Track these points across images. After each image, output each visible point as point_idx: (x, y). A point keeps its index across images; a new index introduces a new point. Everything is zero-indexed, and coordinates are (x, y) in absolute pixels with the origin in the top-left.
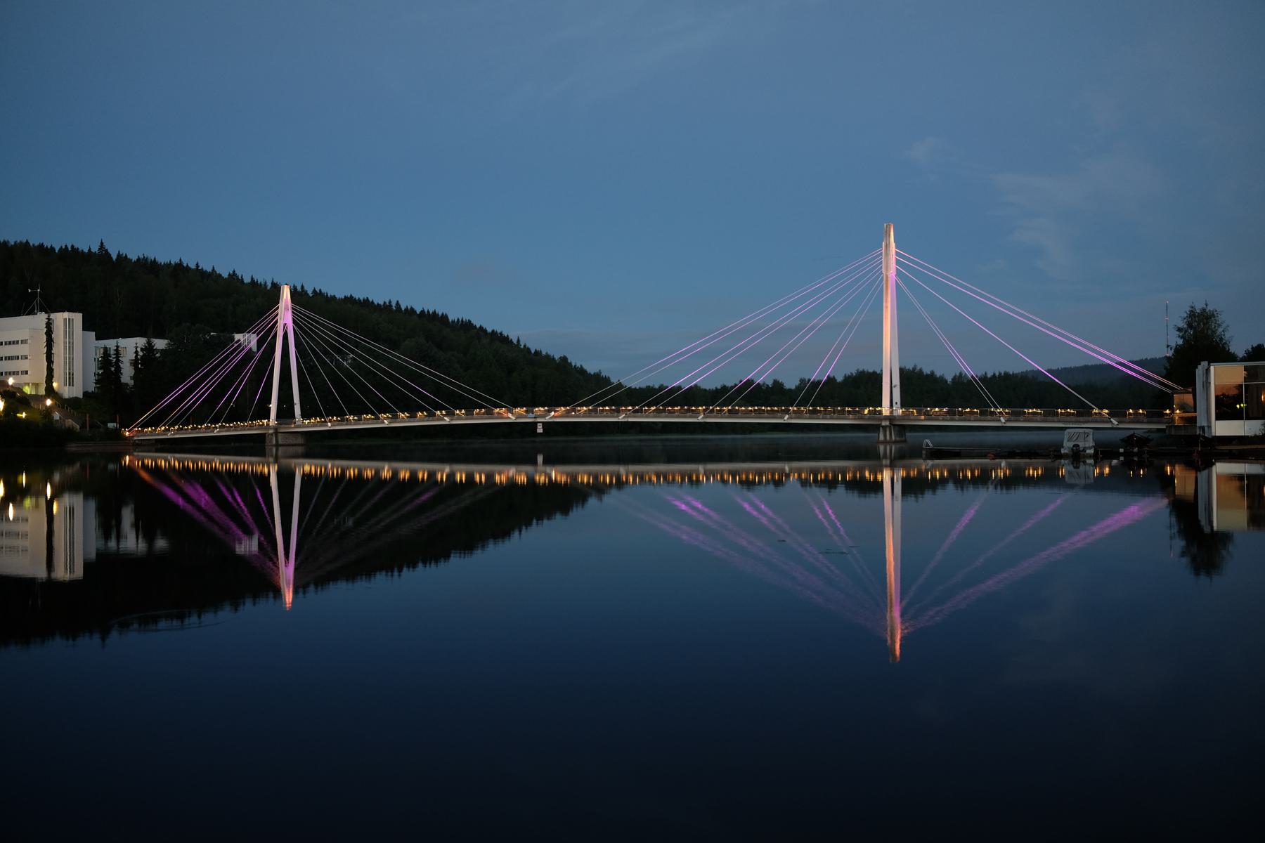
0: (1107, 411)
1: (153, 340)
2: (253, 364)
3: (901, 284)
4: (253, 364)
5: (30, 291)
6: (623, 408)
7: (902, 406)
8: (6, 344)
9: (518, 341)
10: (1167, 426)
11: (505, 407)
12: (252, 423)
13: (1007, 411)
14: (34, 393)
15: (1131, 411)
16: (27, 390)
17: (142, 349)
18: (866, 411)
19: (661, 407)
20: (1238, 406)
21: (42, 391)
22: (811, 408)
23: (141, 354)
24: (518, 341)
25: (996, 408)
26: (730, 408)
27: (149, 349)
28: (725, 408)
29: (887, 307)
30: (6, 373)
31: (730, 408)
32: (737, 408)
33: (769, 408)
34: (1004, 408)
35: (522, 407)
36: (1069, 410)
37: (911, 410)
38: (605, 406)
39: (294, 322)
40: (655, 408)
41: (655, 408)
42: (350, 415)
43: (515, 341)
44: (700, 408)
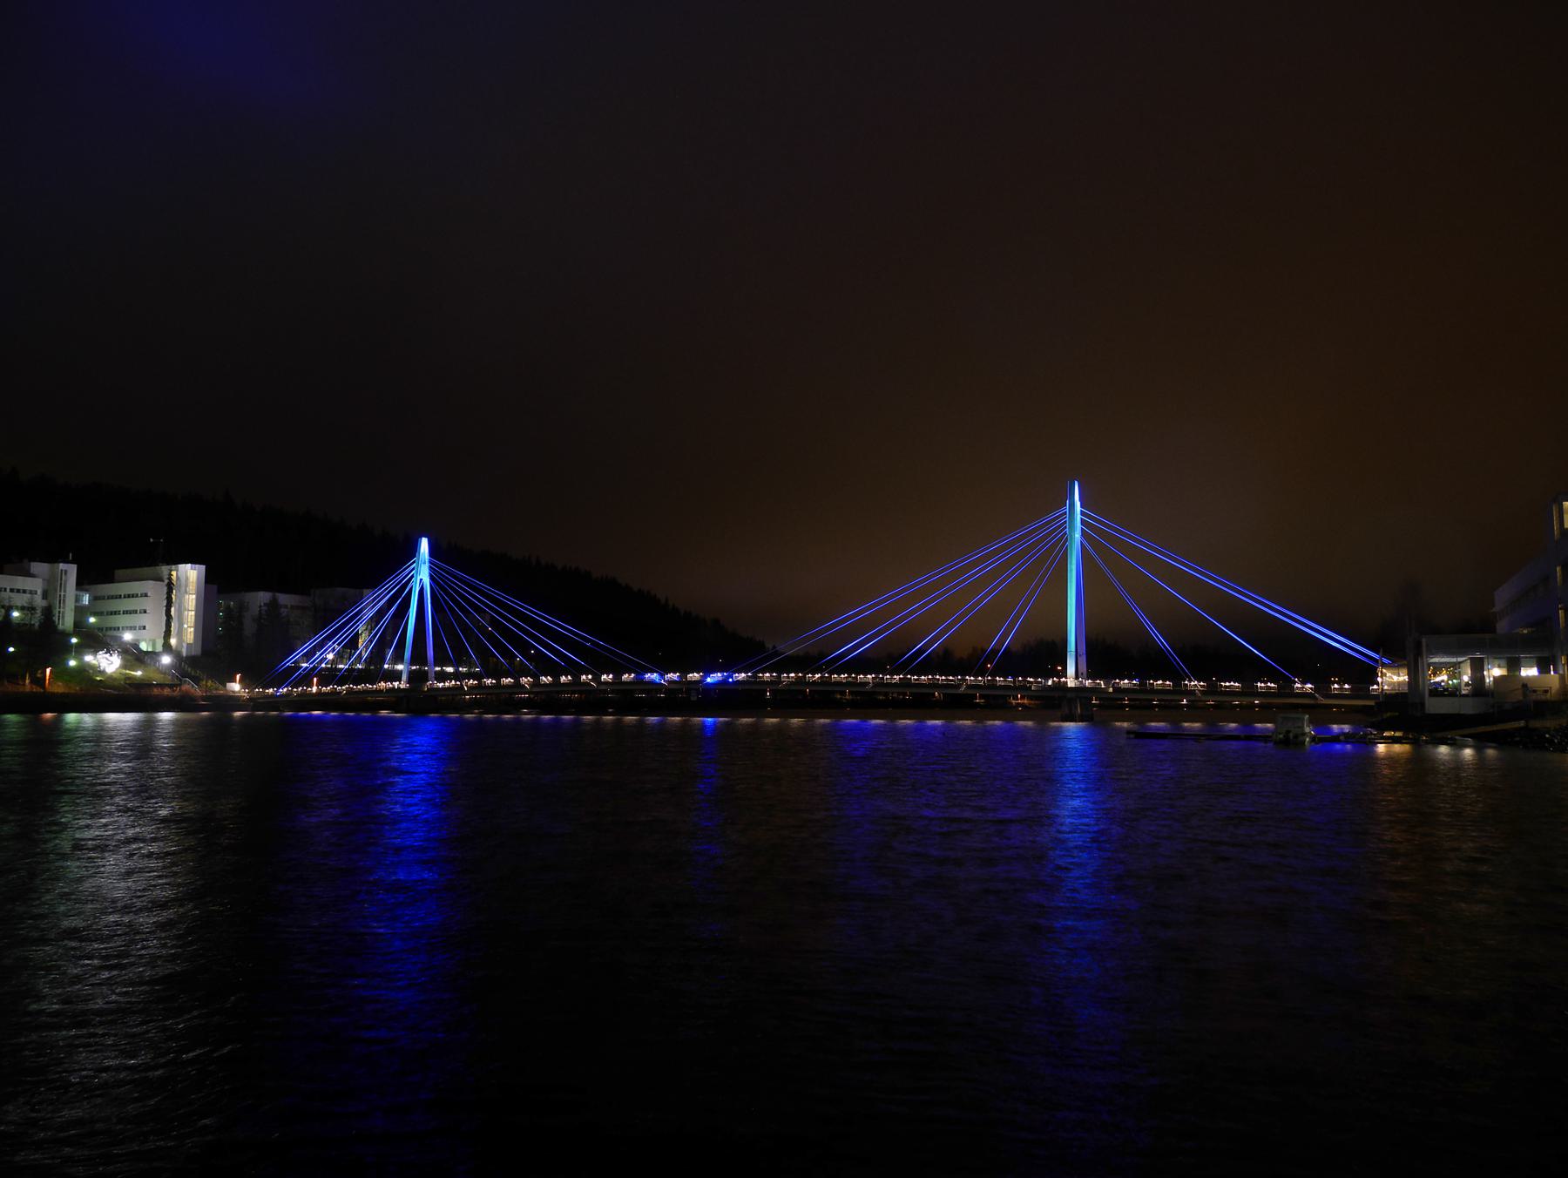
0: (1310, 686)
1: (278, 595)
2: (381, 627)
3: (1086, 544)
4: (381, 627)
5: (151, 540)
6: (785, 675)
7: (1077, 677)
8: (125, 597)
9: (667, 600)
10: (1376, 703)
11: (656, 672)
12: (779, 677)
13: (1202, 683)
14: (150, 650)
15: (1020, 679)
16: (144, 646)
17: (265, 604)
18: (1050, 682)
19: (826, 675)
20: (569, 677)
21: (159, 648)
22: (989, 678)
23: (265, 608)
24: (667, 600)
25: (1190, 681)
26: (901, 676)
27: (273, 604)
28: (895, 677)
29: (1071, 570)
30: (123, 628)
31: (901, 676)
32: (909, 676)
33: (943, 678)
34: (1199, 681)
35: (675, 673)
36: (1269, 684)
37: (1098, 681)
38: (492, 687)
39: (431, 577)
40: (819, 675)
41: (819, 675)
42: (488, 678)
43: (663, 601)
44: (869, 676)
